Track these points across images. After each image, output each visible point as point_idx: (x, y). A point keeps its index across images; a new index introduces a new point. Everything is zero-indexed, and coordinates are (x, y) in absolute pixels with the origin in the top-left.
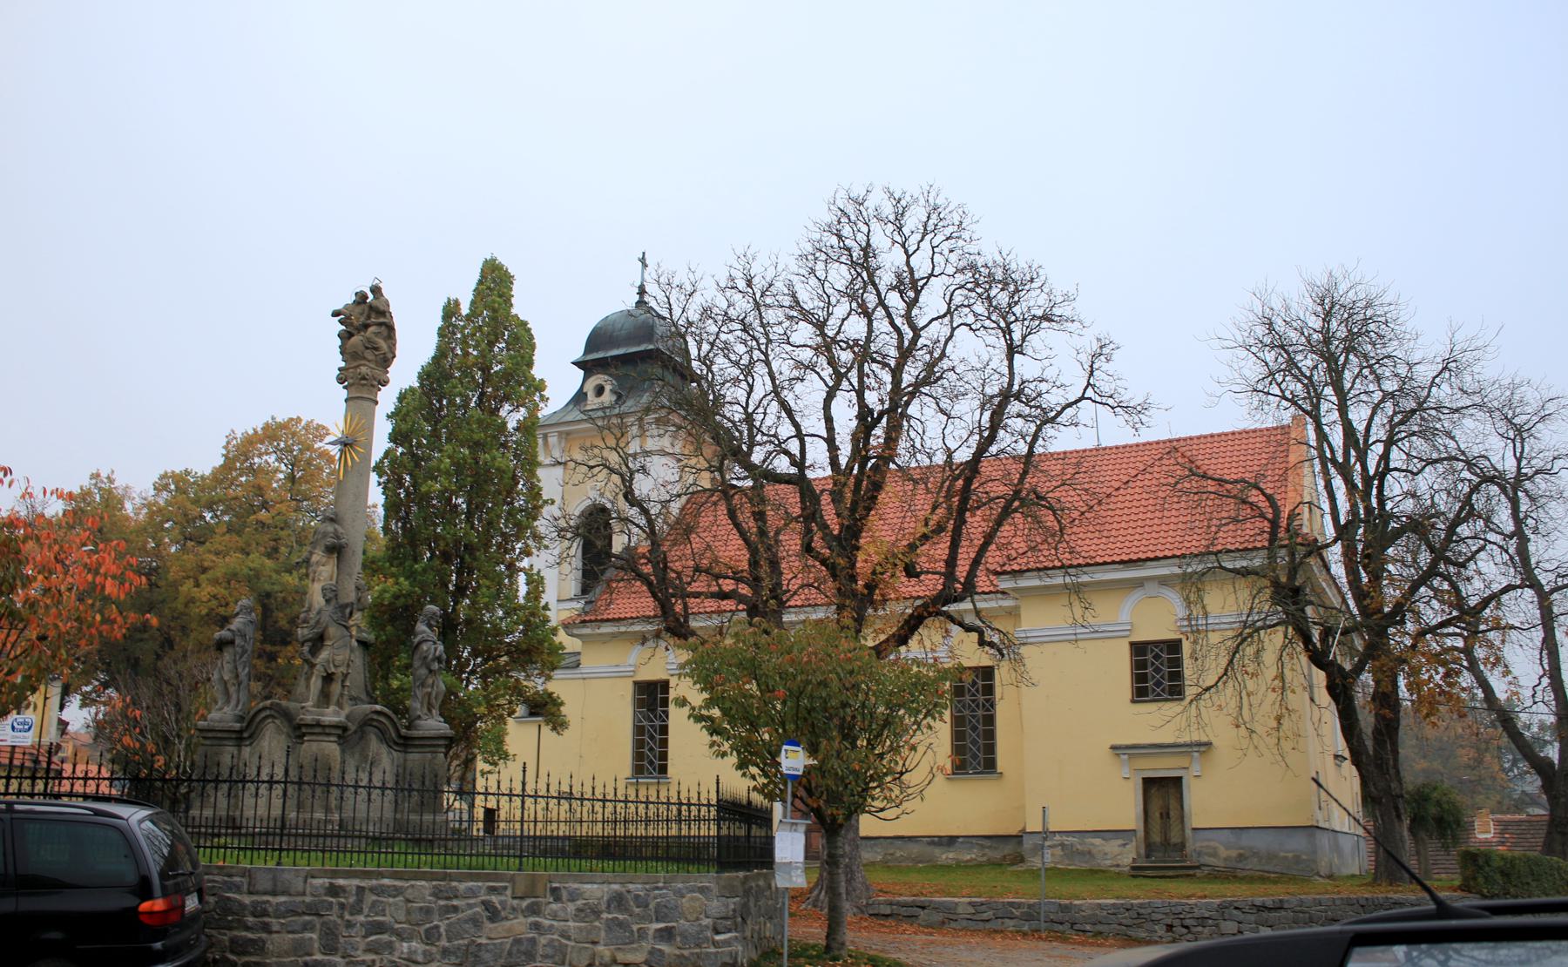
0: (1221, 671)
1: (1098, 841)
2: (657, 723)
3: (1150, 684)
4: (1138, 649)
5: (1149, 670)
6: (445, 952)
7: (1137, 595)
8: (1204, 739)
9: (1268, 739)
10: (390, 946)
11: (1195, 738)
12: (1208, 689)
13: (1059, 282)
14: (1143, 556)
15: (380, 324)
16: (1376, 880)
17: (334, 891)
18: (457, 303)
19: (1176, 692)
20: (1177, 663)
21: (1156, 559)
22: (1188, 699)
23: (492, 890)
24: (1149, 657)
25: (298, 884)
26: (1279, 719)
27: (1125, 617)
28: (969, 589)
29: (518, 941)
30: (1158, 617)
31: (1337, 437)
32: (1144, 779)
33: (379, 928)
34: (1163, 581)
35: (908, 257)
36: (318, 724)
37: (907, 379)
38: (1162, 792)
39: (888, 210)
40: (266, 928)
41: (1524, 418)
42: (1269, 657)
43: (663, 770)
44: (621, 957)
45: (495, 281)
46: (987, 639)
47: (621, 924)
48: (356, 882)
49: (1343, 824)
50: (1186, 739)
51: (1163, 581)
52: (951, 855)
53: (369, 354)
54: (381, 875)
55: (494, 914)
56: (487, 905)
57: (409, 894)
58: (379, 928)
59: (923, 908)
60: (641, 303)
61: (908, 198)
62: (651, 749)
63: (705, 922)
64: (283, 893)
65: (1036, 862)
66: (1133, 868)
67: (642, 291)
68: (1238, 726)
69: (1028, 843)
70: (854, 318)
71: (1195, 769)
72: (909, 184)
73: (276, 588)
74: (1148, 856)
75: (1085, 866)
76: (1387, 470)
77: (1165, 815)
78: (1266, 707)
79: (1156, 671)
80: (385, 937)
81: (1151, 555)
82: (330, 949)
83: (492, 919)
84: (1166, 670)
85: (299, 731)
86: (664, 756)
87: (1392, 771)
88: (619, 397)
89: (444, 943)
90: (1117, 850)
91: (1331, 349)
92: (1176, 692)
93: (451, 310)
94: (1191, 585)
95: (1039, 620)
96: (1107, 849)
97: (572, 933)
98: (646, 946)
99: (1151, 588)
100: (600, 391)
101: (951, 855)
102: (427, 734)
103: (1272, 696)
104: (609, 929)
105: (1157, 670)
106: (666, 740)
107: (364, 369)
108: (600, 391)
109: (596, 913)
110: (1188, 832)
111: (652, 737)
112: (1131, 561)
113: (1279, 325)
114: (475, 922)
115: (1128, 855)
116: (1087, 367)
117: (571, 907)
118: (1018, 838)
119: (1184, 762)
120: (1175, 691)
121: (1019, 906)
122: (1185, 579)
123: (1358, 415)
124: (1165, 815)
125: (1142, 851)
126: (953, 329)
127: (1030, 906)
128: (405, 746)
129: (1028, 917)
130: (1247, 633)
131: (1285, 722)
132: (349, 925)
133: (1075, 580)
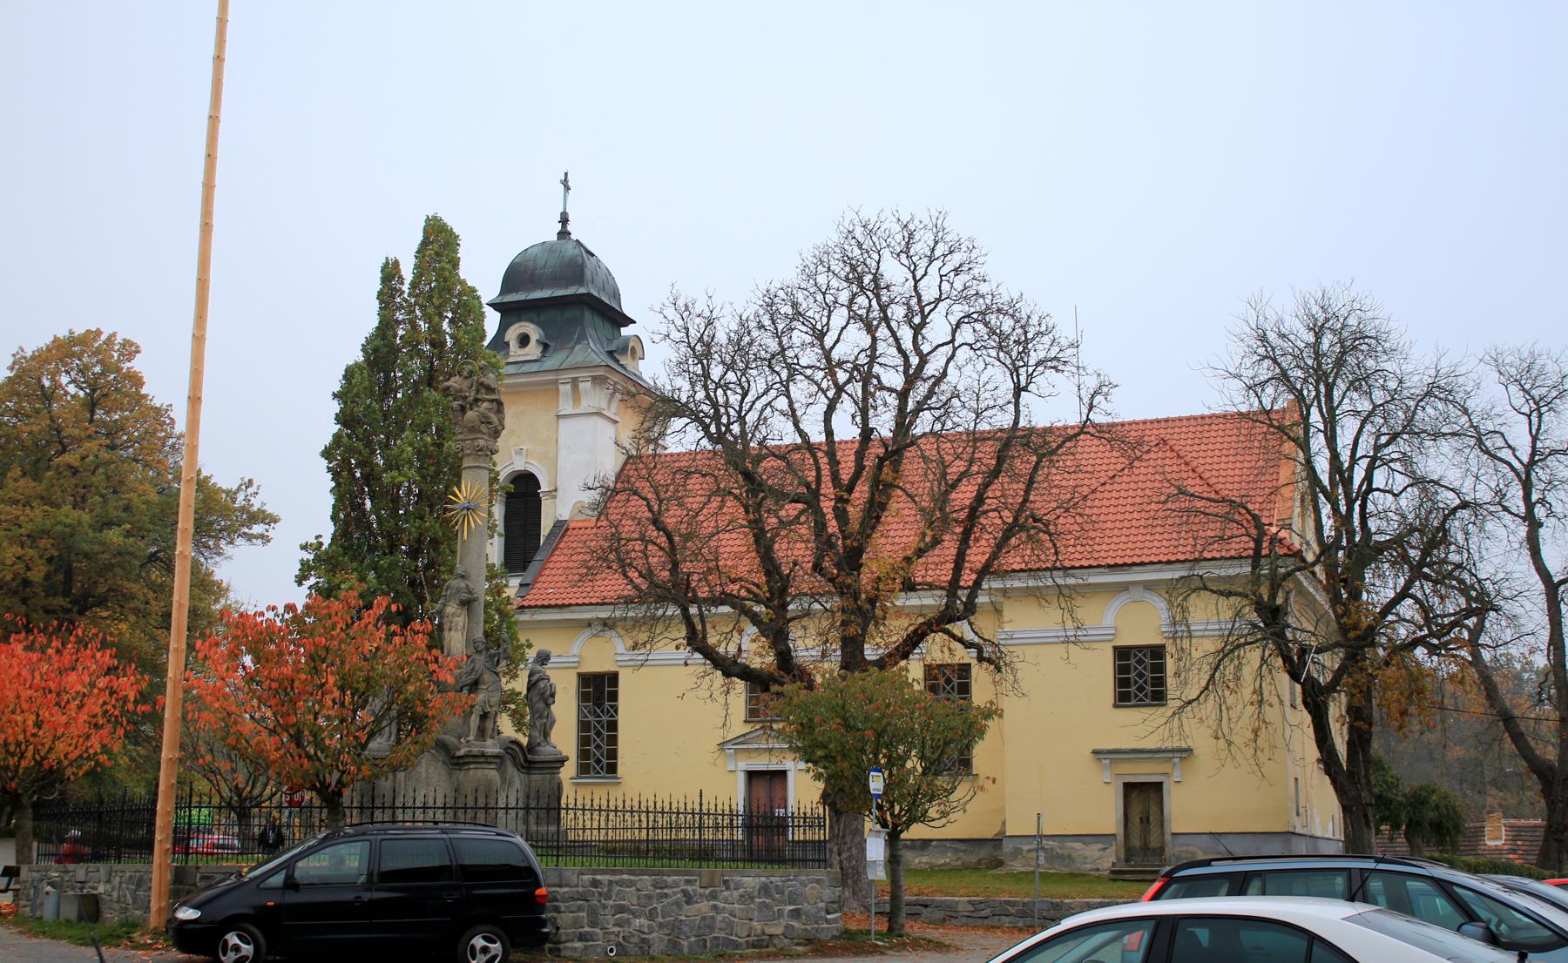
0: (1203, 683)
1: (1078, 845)
2: (605, 718)
3: (1133, 689)
4: (1122, 653)
5: (1132, 675)
6: (661, 926)
7: (1123, 598)
8: (1184, 746)
9: (1245, 750)
10: (628, 922)
11: (1176, 745)
12: (1190, 702)
13: (1065, 333)
14: (1129, 561)
15: (492, 401)
16: (578, 777)
17: (595, 883)
18: (396, 263)
19: (1159, 697)
20: (1160, 668)
21: (1142, 564)
22: (1173, 705)
23: (688, 882)
24: (1133, 661)
25: (574, 880)
26: (1256, 732)
27: (1109, 620)
28: (970, 608)
29: (704, 918)
30: (1143, 623)
31: (1322, 465)
32: (1125, 784)
33: (621, 909)
34: (1149, 586)
35: (916, 282)
36: (483, 755)
37: (911, 406)
38: (1142, 797)
39: (898, 240)
40: (557, 910)
41: (1544, 391)
42: (1248, 673)
43: (612, 769)
44: (767, 931)
45: (439, 243)
46: (986, 655)
47: (767, 906)
48: (607, 877)
49: (1325, 829)
50: (1168, 745)
51: (1149, 586)
52: (924, 859)
53: (484, 428)
54: (622, 872)
55: (689, 899)
56: (685, 892)
57: (639, 885)
58: (621, 909)
59: (926, 906)
60: (564, 234)
61: (916, 222)
62: (598, 747)
63: (822, 905)
64: (567, 885)
65: (1018, 866)
66: (1113, 872)
67: (564, 220)
68: (1217, 738)
69: (1007, 847)
70: (853, 327)
71: (1176, 776)
72: (918, 210)
73: (97, 548)
74: (1127, 860)
75: (1065, 870)
76: (1370, 490)
77: (1145, 820)
78: (1245, 720)
79: (1140, 676)
80: (625, 915)
81: (1137, 560)
82: (593, 924)
83: (688, 903)
84: (1149, 688)
85: (457, 762)
86: (613, 754)
87: (1363, 781)
88: (546, 347)
89: (660, 919)
90: (1096, 854)
91: (1326, 363)
92: (1159, 697)
93: (390, 272)
94: (1179, 592)
95: (1022, 624)
96: (1087, 853)
97: (737, 913)
98: (783, 922)
99: (1137, 593)
100: (524, 340)
101: (924, 859)
102: (548, 758)
103: (1251, 709)
104: (760, 910)
105: (1141, 675)
106: (615, 737)
107: (482, 442)
108: (524, 340)
109: (752, 898)
110: (1168, 837)
111: (598, 734)
112: (1116, 565)
113: (1272, 336)
114: (677, 904)
115: (1107, 859)
116: (1086, 400)
117: (736, 894)
118: (997, 842)
119: (1165, 768)
120: (1158, 697)
121: (1013, 904)
122: (1169, 588)
123: (1344, 439)
124: (1145, 820)
125: (1122, 856)
126: (955, 349)
127: (1024, 904)
128: (529, 768)
129: (1023, 915)
130: (1229, 650)
131: (1262, 733)
132: (605, 907)
133: (1062, 583)
